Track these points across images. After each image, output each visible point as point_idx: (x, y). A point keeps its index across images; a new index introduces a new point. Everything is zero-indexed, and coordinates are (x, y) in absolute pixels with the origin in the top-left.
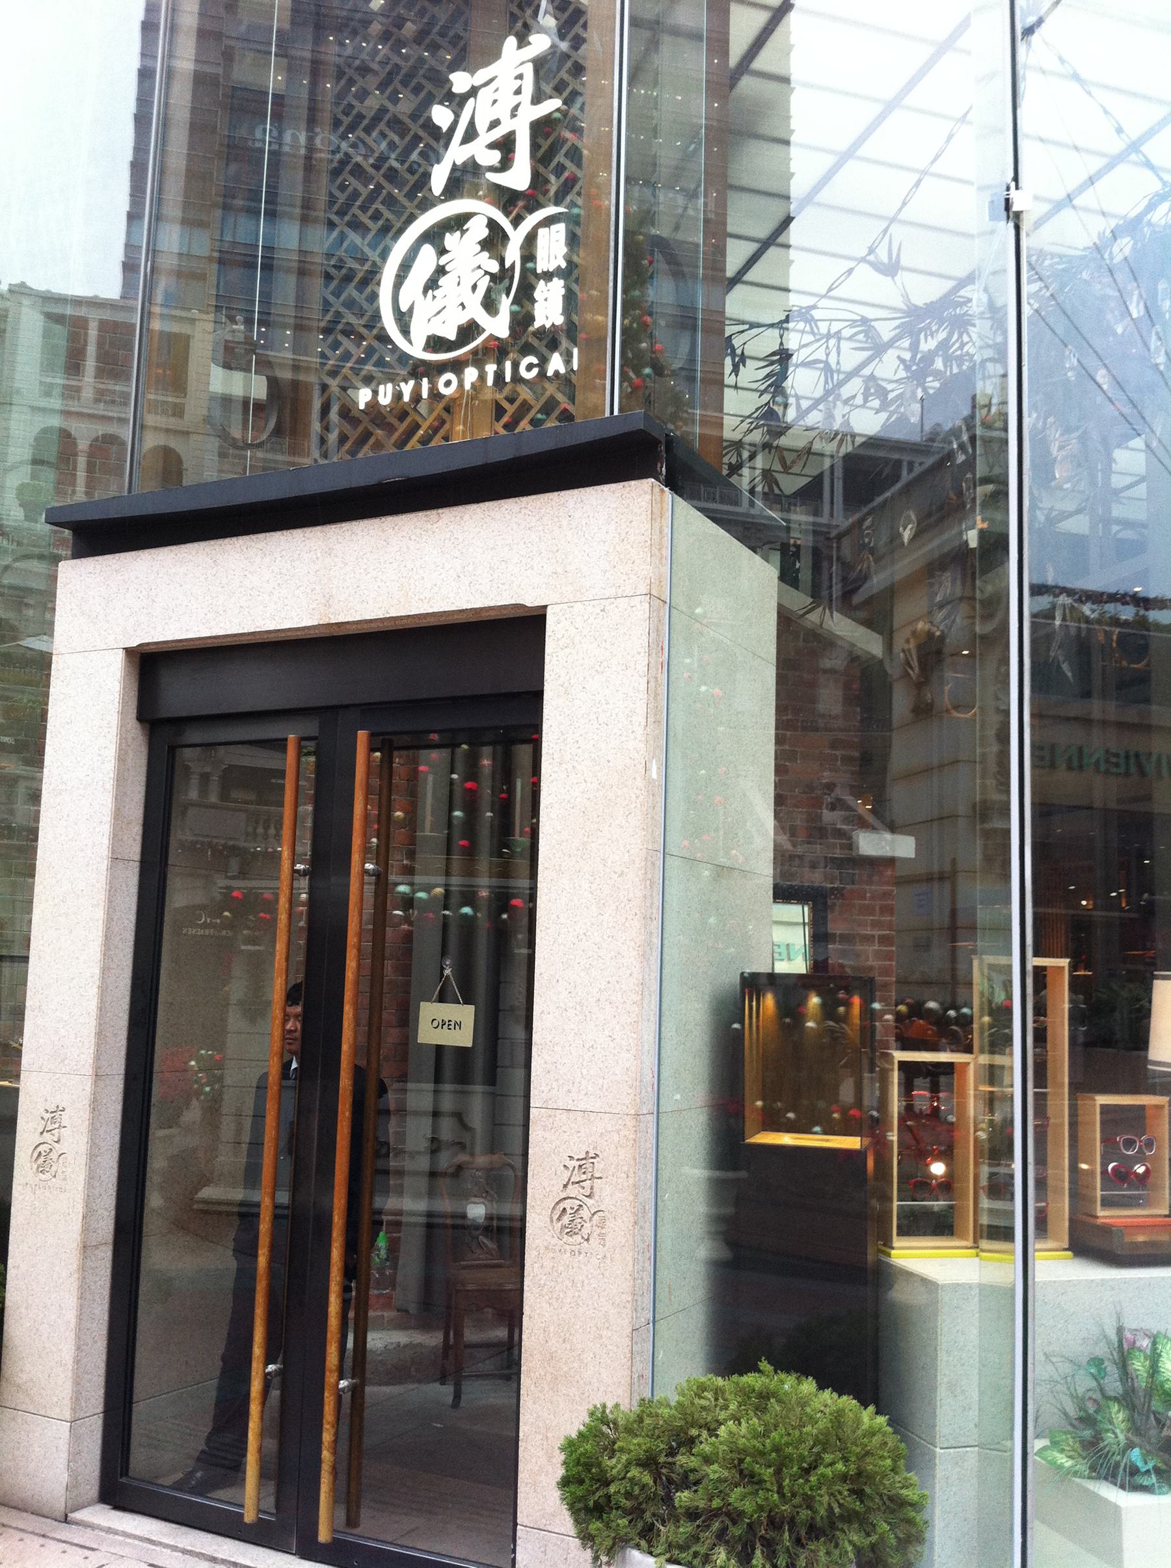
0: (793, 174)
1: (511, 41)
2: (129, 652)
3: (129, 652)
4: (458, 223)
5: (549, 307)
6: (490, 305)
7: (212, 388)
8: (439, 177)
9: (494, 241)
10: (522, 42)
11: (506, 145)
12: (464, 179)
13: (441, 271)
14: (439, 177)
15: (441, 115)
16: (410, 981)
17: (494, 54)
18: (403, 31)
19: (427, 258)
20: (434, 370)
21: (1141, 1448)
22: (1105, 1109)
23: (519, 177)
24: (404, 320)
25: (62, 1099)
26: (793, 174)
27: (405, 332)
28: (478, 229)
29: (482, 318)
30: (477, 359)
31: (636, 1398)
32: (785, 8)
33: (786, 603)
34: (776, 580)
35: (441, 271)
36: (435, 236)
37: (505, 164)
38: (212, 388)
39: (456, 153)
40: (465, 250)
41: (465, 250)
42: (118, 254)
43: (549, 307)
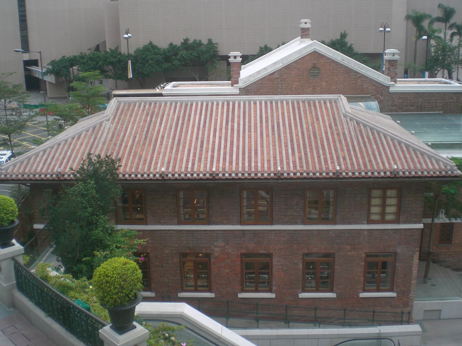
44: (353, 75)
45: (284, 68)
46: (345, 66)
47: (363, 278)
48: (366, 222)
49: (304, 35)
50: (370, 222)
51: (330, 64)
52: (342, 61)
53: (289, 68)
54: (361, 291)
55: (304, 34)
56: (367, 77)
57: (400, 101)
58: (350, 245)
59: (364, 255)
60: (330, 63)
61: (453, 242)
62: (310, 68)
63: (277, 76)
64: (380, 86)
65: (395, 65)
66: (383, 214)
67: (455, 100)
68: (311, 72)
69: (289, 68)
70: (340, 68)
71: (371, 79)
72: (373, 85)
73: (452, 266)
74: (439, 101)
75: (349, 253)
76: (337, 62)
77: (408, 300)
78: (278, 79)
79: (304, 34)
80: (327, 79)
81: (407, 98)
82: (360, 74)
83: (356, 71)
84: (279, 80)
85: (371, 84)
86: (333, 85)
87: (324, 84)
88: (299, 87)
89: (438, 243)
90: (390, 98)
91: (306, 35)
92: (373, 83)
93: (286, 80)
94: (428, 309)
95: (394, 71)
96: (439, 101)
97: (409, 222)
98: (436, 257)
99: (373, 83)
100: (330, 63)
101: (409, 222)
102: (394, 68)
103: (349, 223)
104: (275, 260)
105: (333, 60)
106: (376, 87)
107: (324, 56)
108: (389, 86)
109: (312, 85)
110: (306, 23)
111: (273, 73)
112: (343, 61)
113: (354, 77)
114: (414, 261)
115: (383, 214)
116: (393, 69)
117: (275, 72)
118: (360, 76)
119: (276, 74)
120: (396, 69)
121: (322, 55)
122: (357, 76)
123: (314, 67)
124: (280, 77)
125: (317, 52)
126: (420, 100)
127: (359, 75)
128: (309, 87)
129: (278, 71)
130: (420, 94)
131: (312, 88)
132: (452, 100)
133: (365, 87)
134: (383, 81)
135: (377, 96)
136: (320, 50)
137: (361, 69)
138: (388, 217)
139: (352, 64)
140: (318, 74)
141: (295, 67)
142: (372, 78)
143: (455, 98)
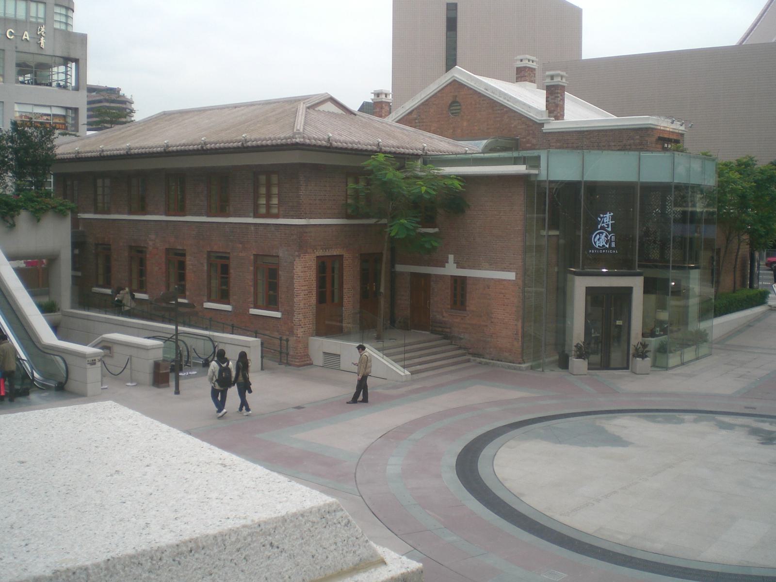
0: (444, 267)
1: (608, 213)
2: (586, 287)
3: (586, 287)
4: (602, 233)
5: (613, 245)
6: (606, 244)
7: (514, 278)
8: (599, 227)
9: (606, 236)
10: (610, 213)
12: (602, 228)
13: (600, 238)
14: (599, 227)
15: (599, 219)
17: (606, 214)
19: (598, 236)
20: (599, 250)
21: (26, 209)
24: (595, 243)
26: (444, 267)
27: (596, 245)
28: (604, 234)
29: (605, 245)
30: (604, 249)
33: (14, 267)
34: (70, 270)
35: (600, 238)
36: (599, 233)
37: (608, 227)
38: (514, 278)
40: (603, 237)
41: (603, 237)
42: (618, 153)
44: (499, 110)
45: (423, 104)
46: (489, 97)
47: (252, 288)
48: (252, 214)
49: (519, 77)
50: (256, 215)
51: (471, 96)
52: (485, 91)
53: (427, 105)
54: (252, 306)
55: (519, 75)
56: (515, 112)
57: (558, 144)
58: (241, 243)
59: (252, 257)
60: (471, 94)
61: (467, 308)
62: (450, 102)
63: (415, 116)
64: (531, 124)
65: (555, 93)
66: (268, 206)
67: (638, 141)
68: (452, 108)
69: (427, 105)
70: (483, 100)
71: (521, 115)
72: (523, 123)
73: (470, 349)
74: (613, 144)
75: (241, 254)
76: (480, 93)
77: (293, 325)
78: (416, 119)
79: (519, 75)
80: (469, 117)
81: (568, 140)
82: (506, 107)
83: (505, 106)
84: (417, 121)
85: (520, 121)
86: (476, 124)
87: (465, 124)
88: (438, 130)
89: (449, 306)
90: (545, 141)
91: (521, 77)
92: (523, 119)
93: (424, 121)
94: (332, 352)
95: (553, 101)
96: (613, 144)
97: (287, 216)
98: (448, 330)
99: (523, 119)
100: (471, 94)
101: (287, 216)
102: (553, 97)
103: (240, 216)
104: (188, 258)
105: (475, 90)
106: (526, 125)
107: (465, 86)
108: (543, 124)
109: (452, 126)
110: (521, 60)
111: (411, 113)
112: (487, 92)
113: (499, 112)
114: (294, 270)
115: (268, 206)
116: (552, 99)
117: (413, 111)
118: (506, 111)
119: (414, 113)
120: (557, 98)
121: (462, 84)
122: (502, 111)
123: (454, 102)
124: (419, 117)
125: (458, 81)
126: (585, 143)
127: (505, 109)
128: (448, 129)
129: (416, 109)
130: (586, 133)
131: (452, 131)
132: (632, 141)
133: (513, 126)
134: (534, 116)
135: (528, 138)
136: (494, 86)
137: (508, 101)
138: (275, 211)
139: (496, 94)
140: (459, 111)
141: (434, 103)
142: (521, 113)
143: (638, 137)
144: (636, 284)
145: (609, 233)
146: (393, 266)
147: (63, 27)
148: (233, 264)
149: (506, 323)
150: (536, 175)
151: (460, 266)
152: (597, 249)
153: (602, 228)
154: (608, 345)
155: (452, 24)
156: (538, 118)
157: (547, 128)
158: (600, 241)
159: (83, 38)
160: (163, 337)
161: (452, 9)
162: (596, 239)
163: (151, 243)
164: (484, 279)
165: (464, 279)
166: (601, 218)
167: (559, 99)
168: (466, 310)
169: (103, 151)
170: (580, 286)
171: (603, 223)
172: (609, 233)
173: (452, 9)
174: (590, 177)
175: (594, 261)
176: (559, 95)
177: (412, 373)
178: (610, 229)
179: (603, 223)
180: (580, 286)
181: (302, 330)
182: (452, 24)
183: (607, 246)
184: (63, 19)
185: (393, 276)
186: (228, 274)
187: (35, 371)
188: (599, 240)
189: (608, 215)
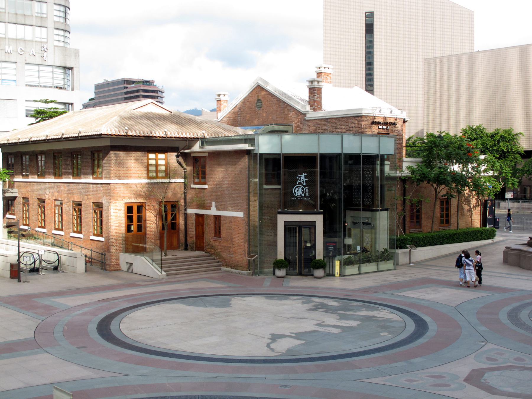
4: (300, 187)
5: (307, 194)
6: (303, 193)
7: (242, 216)
11: (303, 181)
16: (3, 188)
18: (133, 161)
19: (297, 189)
22: (312, 225)
23: (305, 184)
24: (295, 193)
25: (167, 98)
31: (307, 314)
32: (22, 157)
36: (298, 187)
38: (242, 216)
39: (299, 181)
40: (300, 189)
41: (300, 189)
43: (307, 194)
67: (356, 125)
74: (343, 127)
132: (353, 125)
144: (319, 219)
145: (305, 186)
146: (186, 210)
147: (62, 44)
148: (83, 208)
149: (238, 244)
150: (253, 150)
151: (218, 209)
152: (296, 197)
153: (300, 183)
154: (302, 262)
155: (369, 28)
156: (302, 110)
157: (308, 116)
158: (298, 192)
159: (76, 53)
160: (176, 274)
161: (370, 16)
162: (296, 191)
163: (47, 196)
164: (230, 217)
165: (219, 217)
166: (299, 177)
167: (316, 97)
168: (220, 237)
169: (9, 140)
170: (282, 219)
171: (300, 180)
172: (305, 186)
173: (370, 16)
174: (323, 151)
175: (289, 204)
176: (316, 94)
177: (168, 275)
178: (305, 184)
179: (300, 180)
180: (282, 219)
181: (114, 248)
182: (369, 28)
183: (303, 195)
184: (62, 39)
185: (186, 214)
186: (128, 216)
187: (302, 344)
188: (298, 191)
189: (303, 175)
